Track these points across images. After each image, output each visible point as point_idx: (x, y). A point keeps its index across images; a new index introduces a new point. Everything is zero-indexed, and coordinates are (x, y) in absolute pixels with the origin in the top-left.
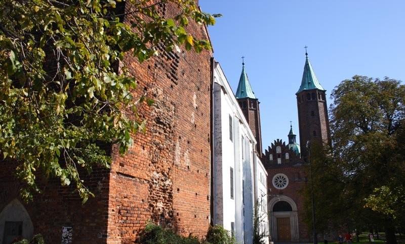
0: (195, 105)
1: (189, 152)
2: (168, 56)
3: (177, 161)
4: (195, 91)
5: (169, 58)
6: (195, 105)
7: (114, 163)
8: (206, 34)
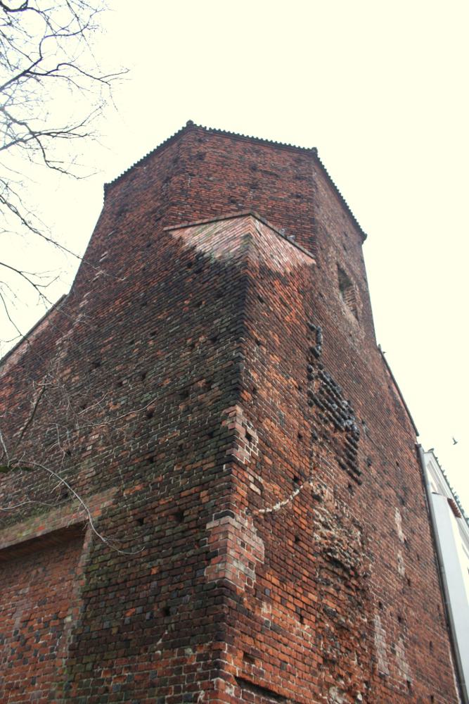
4: (397, 505)
7: (230, 650)
8: (399, 398)
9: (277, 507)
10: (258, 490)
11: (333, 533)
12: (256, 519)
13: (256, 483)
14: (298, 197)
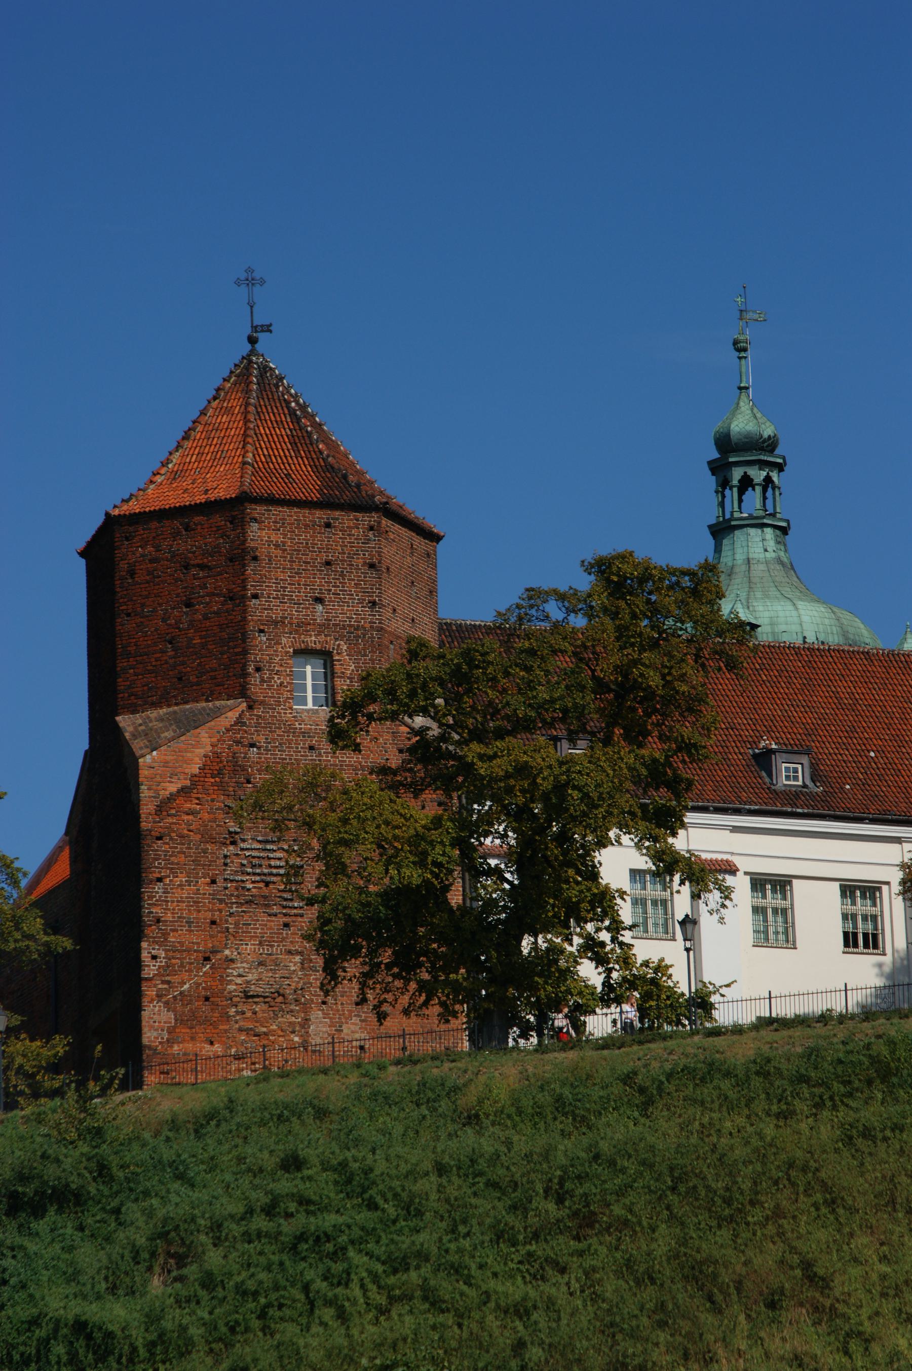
1: (361, 1021)
2: (262, 881)
5: (267, 884)
9: (186, 987)
10: (166, 986)
12: (166, 1003)
13: (163, 982)
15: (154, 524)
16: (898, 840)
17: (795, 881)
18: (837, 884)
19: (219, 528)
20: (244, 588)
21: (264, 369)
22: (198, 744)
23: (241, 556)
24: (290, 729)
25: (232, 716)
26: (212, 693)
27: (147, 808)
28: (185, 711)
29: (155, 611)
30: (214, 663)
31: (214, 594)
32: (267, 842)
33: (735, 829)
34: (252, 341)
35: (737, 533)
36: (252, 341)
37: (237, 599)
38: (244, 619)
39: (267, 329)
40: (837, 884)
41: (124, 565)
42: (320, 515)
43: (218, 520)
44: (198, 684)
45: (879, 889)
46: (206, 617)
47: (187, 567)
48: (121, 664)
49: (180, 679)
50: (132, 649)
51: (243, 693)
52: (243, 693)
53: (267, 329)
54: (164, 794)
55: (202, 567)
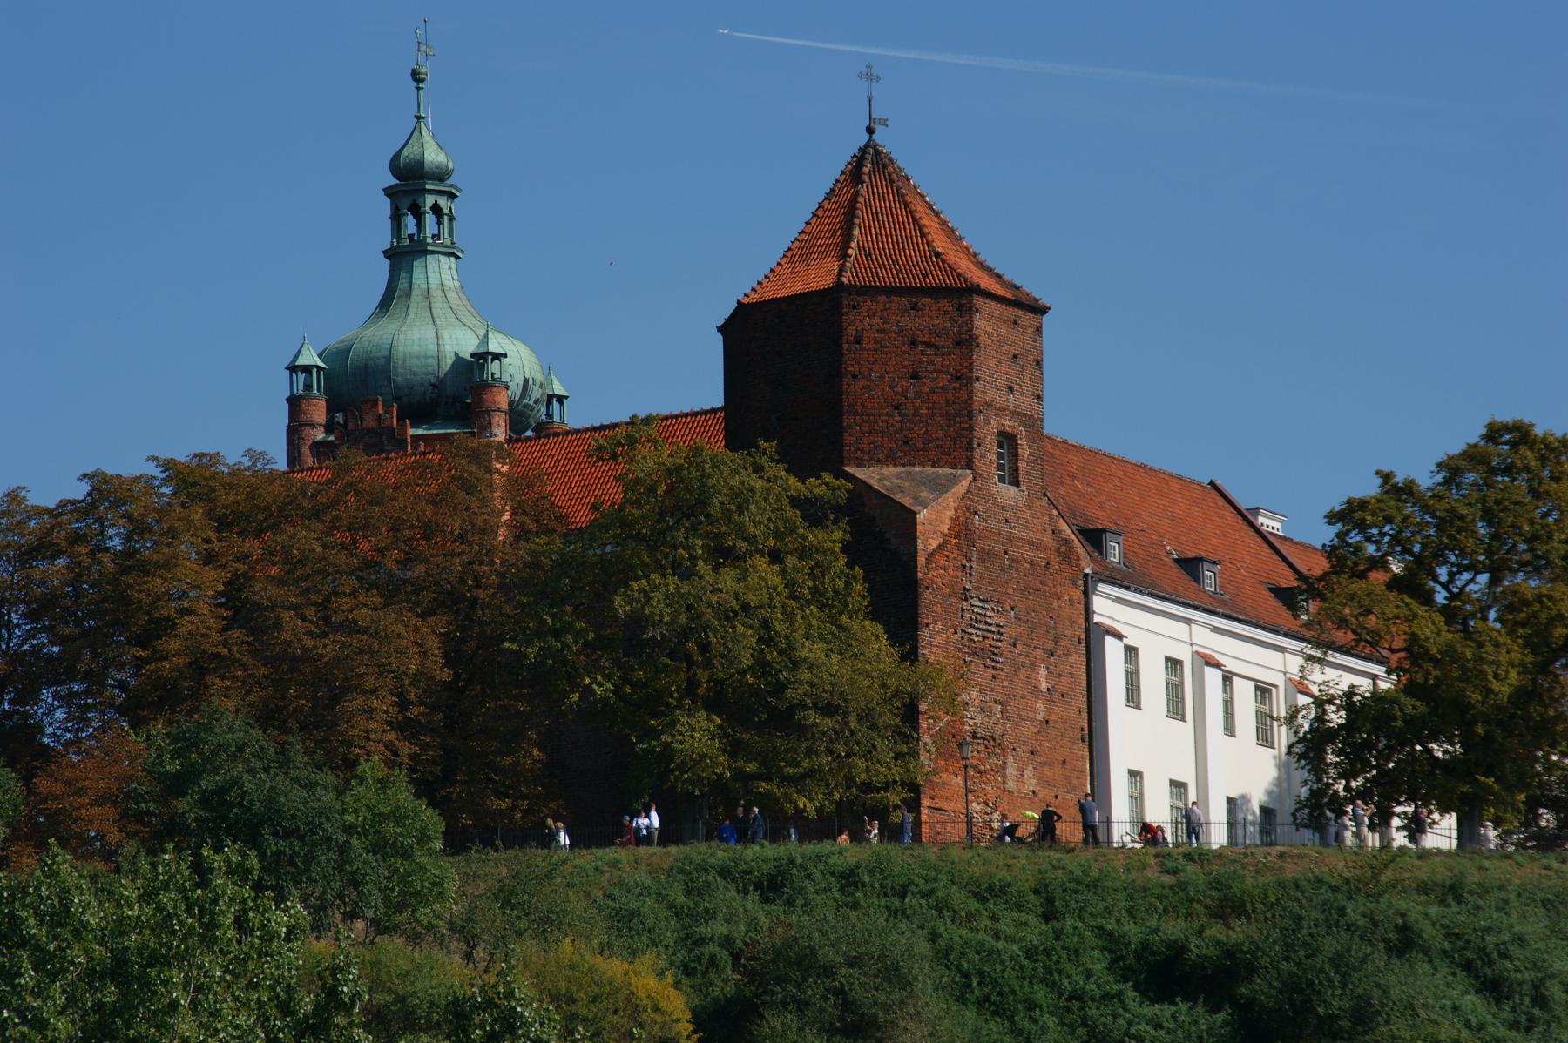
0: (1044, 686)
3: (1011, 784)
6: (1044, 686)
11: (978, 721)
14: (958, 378)
15: (883, 298)
16: (1282, 650)
17: (1236, 679)
18: (1252, 684)
19: (946, 313)
20: (971, 371)
21: (878, 153)
22: (947, 508)
23: (966, 342)
24: (996, 504)
25: (965, 483)
26: (939, 461)
27: (921, 560)
28: (937, 475)
29: (882, 377)
30: (940, 435)
31: (939, 371)
32: (985, 601)
33: (1216, 630)
34: (870, 131)
35: (429, 257)
36: (870, 131)
37: (964, 379)
38: (971, 398)
39: (884, 123)
40: (1252, 684)
41: (851, 330)
42: (1011, 312)
43: (945, 304)
44: (924, 450)
45: (1269, 691)
46: (932, 391)
47: (913, 343)
48: (847, 420)
49: (906, 443)
50: (858, 408)
51: (969, 465)
52: (969, 465)
53: (884, 123)
54: (930, 548)
55: (928, 345)
